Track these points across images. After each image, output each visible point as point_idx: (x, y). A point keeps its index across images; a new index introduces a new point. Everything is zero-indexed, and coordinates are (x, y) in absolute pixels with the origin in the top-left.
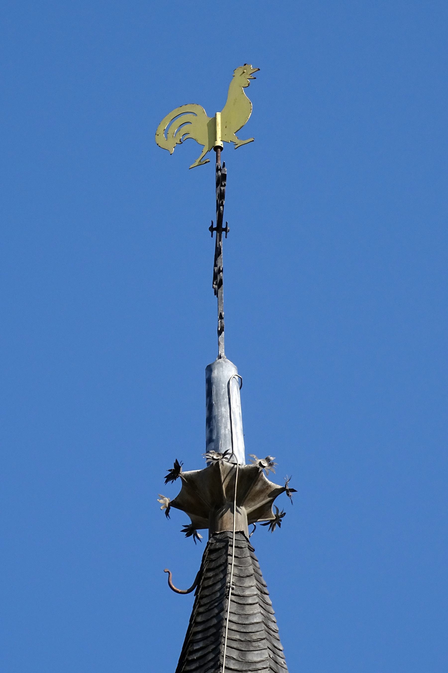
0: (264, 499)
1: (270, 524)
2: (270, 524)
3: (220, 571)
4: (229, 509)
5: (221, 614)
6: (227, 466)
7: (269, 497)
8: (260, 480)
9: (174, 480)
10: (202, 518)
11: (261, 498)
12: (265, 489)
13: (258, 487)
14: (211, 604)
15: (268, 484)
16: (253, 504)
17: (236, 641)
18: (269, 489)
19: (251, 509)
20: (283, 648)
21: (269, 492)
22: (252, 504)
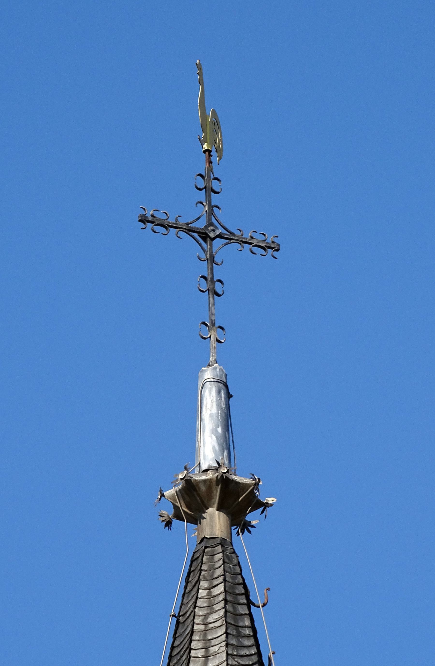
0: (217, 492)
1: (263, 507)
2: (263, 507)
3: (208, 571)
4: (245, 530)
5: (236, 635)
6: (172, 494)
7: (219, 486)
8: (198, 484)
9: (220, 545)
10: (207, 546)
11: (215, 492)
12: (210, 484)
13: (203, 488)
14: (221, 617)
15: (208, 479)
16: (214, 500)
17: (222, 626)
18: (213, 481)
19: (216, 505)
20: (248, 613)
21: (214, 483)
22: (213, 501)
